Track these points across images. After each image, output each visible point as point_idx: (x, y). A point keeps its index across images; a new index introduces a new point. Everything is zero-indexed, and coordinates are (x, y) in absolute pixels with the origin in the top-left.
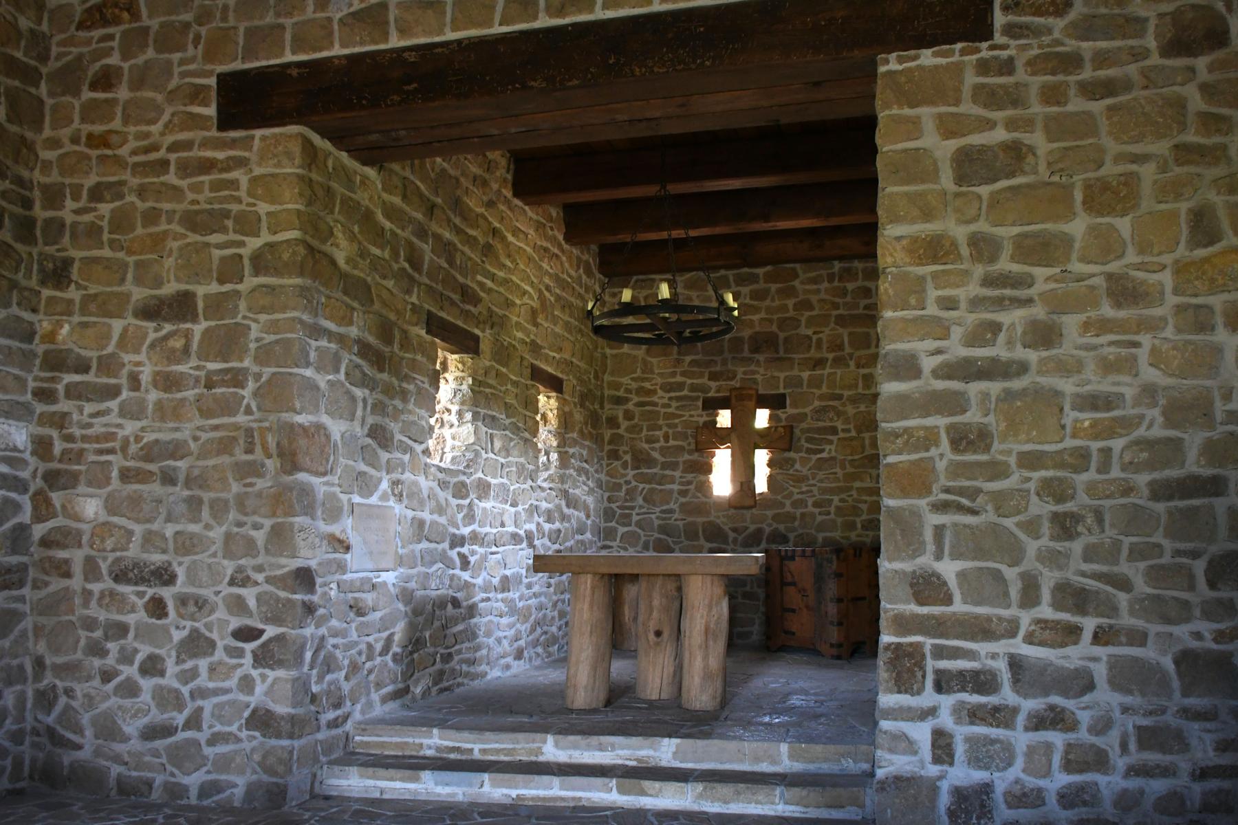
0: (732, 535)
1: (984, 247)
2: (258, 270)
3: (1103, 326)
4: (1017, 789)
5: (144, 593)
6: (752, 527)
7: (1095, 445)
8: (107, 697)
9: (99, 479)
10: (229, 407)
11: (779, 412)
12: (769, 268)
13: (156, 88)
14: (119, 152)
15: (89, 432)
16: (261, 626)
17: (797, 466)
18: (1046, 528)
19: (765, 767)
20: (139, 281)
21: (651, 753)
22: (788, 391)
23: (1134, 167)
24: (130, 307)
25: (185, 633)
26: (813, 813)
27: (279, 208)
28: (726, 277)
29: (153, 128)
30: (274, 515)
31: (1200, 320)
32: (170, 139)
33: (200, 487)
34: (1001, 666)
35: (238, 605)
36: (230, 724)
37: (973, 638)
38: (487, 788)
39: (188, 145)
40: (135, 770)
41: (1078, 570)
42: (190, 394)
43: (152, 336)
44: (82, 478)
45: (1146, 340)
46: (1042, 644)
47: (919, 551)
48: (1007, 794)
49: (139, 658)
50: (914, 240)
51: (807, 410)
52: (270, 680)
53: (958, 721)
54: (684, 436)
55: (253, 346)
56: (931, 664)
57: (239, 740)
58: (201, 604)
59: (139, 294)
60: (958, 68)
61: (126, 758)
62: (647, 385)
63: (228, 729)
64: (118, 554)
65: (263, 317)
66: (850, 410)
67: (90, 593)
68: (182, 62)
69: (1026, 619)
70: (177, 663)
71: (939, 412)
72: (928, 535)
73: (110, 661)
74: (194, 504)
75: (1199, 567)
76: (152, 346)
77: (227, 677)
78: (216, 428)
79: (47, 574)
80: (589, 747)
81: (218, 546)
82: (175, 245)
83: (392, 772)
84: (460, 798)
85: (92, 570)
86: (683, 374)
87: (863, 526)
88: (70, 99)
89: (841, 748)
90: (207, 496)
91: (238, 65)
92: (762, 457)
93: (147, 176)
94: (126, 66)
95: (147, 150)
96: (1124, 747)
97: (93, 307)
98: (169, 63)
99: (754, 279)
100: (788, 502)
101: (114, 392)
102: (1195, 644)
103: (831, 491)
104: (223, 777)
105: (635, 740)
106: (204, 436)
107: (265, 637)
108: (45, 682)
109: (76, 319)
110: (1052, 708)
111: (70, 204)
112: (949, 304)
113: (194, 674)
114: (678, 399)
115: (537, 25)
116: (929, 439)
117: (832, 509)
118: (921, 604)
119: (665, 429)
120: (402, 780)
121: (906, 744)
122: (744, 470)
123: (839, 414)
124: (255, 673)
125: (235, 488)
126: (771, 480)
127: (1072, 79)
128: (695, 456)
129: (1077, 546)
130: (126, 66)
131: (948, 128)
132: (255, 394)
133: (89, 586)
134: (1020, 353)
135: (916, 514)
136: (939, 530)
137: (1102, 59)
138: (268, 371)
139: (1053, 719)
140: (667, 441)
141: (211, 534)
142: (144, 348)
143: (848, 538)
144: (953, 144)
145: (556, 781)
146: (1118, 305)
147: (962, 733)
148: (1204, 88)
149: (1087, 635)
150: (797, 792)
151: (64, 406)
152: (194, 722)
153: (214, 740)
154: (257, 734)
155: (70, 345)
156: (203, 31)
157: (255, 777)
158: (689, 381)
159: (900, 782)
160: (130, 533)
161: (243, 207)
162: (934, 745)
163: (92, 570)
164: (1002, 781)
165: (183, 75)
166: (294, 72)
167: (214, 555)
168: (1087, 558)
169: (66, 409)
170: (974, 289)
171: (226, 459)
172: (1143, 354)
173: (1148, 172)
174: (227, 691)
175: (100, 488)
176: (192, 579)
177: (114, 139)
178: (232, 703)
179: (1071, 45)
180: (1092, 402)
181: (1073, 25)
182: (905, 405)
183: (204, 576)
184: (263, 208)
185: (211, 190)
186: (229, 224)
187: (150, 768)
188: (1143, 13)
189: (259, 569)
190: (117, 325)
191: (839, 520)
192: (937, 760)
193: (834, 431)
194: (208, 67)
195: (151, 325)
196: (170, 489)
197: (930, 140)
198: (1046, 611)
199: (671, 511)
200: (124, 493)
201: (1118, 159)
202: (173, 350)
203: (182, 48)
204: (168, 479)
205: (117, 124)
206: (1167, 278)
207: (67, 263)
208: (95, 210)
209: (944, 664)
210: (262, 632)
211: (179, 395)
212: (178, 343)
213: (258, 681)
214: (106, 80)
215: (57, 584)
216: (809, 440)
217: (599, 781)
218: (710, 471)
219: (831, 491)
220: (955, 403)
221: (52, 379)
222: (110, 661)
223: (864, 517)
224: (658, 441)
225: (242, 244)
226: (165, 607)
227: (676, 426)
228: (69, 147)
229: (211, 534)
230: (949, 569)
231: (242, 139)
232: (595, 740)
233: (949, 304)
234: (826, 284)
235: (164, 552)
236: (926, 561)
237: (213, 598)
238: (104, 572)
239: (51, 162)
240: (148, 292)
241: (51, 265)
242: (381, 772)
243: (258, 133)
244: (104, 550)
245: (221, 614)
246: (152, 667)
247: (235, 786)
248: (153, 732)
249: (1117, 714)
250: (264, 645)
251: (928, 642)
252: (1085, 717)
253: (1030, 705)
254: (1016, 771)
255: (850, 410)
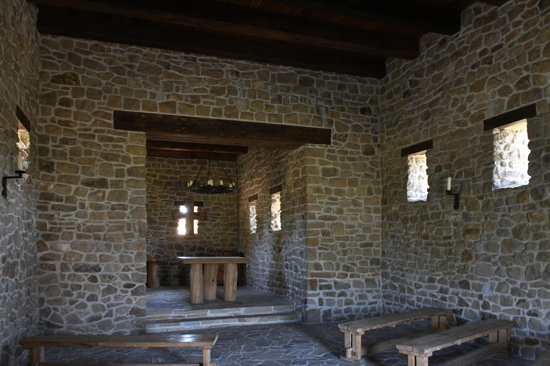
0: (185, 248)
1: (328, 191)
2: (130, 174)
3: (351, 210)
4: (336, 310)
5: (88, 275)
6: (192, 245)
7: (350, 236)
8: (73, 310)
9: (67, 237)
10: (122, 216)
11: (201, 208)
12: (197, 160)
13: (88, 110)
14: (73, 129)
15: (63, 221)
16: (134, 283)
17: (208, 225)
18: (341, 253)
19: (268, 313)
20: (84, 173)
21: (238, 312)
22: (204, 201)
23: (357, 177)
24: (80, 181)
25: (106, 286)
26: (287, 321)
27: (138, 156)
28: (182, 161)
29: (87, 123)
30: (138, 249)
31: (368, 210)
32: (95, 128)
33: (111, 241)
34: (332, 283)
35: (127, 277)
36: (124, 314)
37: (327, 278)
38: (201, 325)
39: (103, 131)
40: (86, 332)
41: (347, 263)
42: (105, 211)
43: (89, 192)
44: (60, 237)
45: (359, 214)
46: (340, 278)
47: (316, 259)
48: (334, 311)
49: (86, 296)
50: (314, 188)
51: (211, 207)
52: (138, 299)
53: (324, 296)
54: (167, 214)
55: (129, 198)
56: (318, 284)
57: (127, 318)
58: (111, 278)
59: (83, 177)
60: (324, 150)
61: (82, 328)
62: (154, 195)
63: (123, 315)
64: (77, 262)
65: (132, 189)
66: (225, 208)
67: (65, 275)
68: (99, 104)
69: (337, 273)
70: (102, 296)
71: (319, 227)
72: (318, 255)
73: (74, 297)
74: (108, 247)
75: (369, 261)
76: (90, 195)
77: (122, 299)
78: (116, 222)
79: (44, 269)
80: (221, 312)
81: (118, 259)
82: (99, 163)
83: (170, 324)
84: (193, 328)
85: (64, 267)
86: (167, 192)
87: (229, 245)
88: (50, 106)
89: (287, 306)
90: (113, 244)
91: (122, 109)
92: (196, 222)
93: (86, 139)
94: (74, 99)
95: (85, 130)
96: (356, 299)
97: (64, 180)
98: (94, 103)
99: (192, 163)
100: (204, 237)
101: (74, 209)
102: (368, 277)
103: (219, 234)
104: (122, 330)
105: (233, 309)
106: (111, 225)
107: (136, 287)
108: (44, 306)
109: (56, 183)
110: (342, 292)
111: (51, 143)
112: (321, 203)
113: (109, 299)
114: (165, 201)
115: (222, 118)
116: (317, 234)
117: (219, 240)
118: (316, 270)
119: (160, 211)
120: (174, 325)
121: (313, 302)
122: (190, 225)
123: (221, 209)
124: (132, 298)
125: (124, 241)
126: (199, 230)
127: (346, 156)
128: (172, 221)
129: (346, 257)
130: (74, 99)
131: (322, 163)
132: (131, 213)
133: (64, 273)
134: (335, 215)
135: (315, 250)
136: (320, 254)
137: (352, 153)
138: (135, 206)
139: (343, 294)
140: (161, 215)
141: (115, 255)
142: (87, 196)
143: (224, 249)
144: (322, 167)
145: (221, 320)
146: (354, 206)
147: (325, 298)
148: (370, 163)
149: (349, 276)
150: (283, 316)
151: (50, 212)
152: (110, 314)
153: (117, 319)
154: (134, 316)
155: (53, 192)
156: (108, 95)
157: (134, 329)
158: (169, 195)
159: (313, 310)
160: (82, 256)
161: (125, 154)
162: (319, 302)
163: (64, 267)
164: (333, 308)
165: (100, 108)
166: (144, 116)
167: (117, 262)
168: (348, 260)
169: (52, 213)
170: (326, 200)
171: (120, 232)
172: (359, 217)
173: (360, 178)
174: (122, 304)
175: (68, 240)
176: (108, 269)
177: (71, 124)
178: (124, 307)
179: (346, 149)
180: (350, 226)
181: (346, 144)
182: (313, 226)
183: (113, 268)
184: (132, 156)
185: (113, 147)
186: (120, 159)
187: (92, 331)
188: (359, 144)
189: (133, 266)
190: (74, 187)
191: (221, 243)
192: (320, 305)
193: (219, 215)
194: (111, 108)
195: (89, 188)
196: (98, 241)
197: (317, 165)
198: (341, 271)
199: (163, 239)
200: (79, 243)
201: (355, 175)
202: (99, 197)
203: (99, 99)
204: (97, 238)
205: (72, 119)
206: (363, 201)
207: (52, 164)
208: (64, 147)
209: (321, 284)
210: (135, 285)
211: (101, 211)
212: (100, 195)
213: (133, 300)
214: (66, 103)
215: (48, 273)
216: (211, 217)
217: (233, 319)
218: (177, 226)
219: (219, 234)
220: (323, 225)
221: (47, 203)
222: (74, 297)
223: (229, 242)
224: (158, 215)
225: (124, 166)
226: (97, 279)
227: (164, 210)
228: (50, 123)
229: (115, 255)
230: (322, 262)
231: (123, 133)
232: (222, 310)
233: (321, 203)
234: (216, 167)
235: (96, 261)
236: (317, 261)
237: (116, 275)
238: (71, 268)
239: (42, 127)
240: (87, 177)
241: (45, 164)
242: (167, 324)
243: (129, 132)
244: (71, 261)
245: (119, 280)
246: (92, 298)
247: (126, 332)
248: (92, 319)
249: (355, 292)
250: (135, 289)
251: (318, 279)
252: (348, 293)
253: (338, 291)
254: (336, 306)
255: (225, 208)
